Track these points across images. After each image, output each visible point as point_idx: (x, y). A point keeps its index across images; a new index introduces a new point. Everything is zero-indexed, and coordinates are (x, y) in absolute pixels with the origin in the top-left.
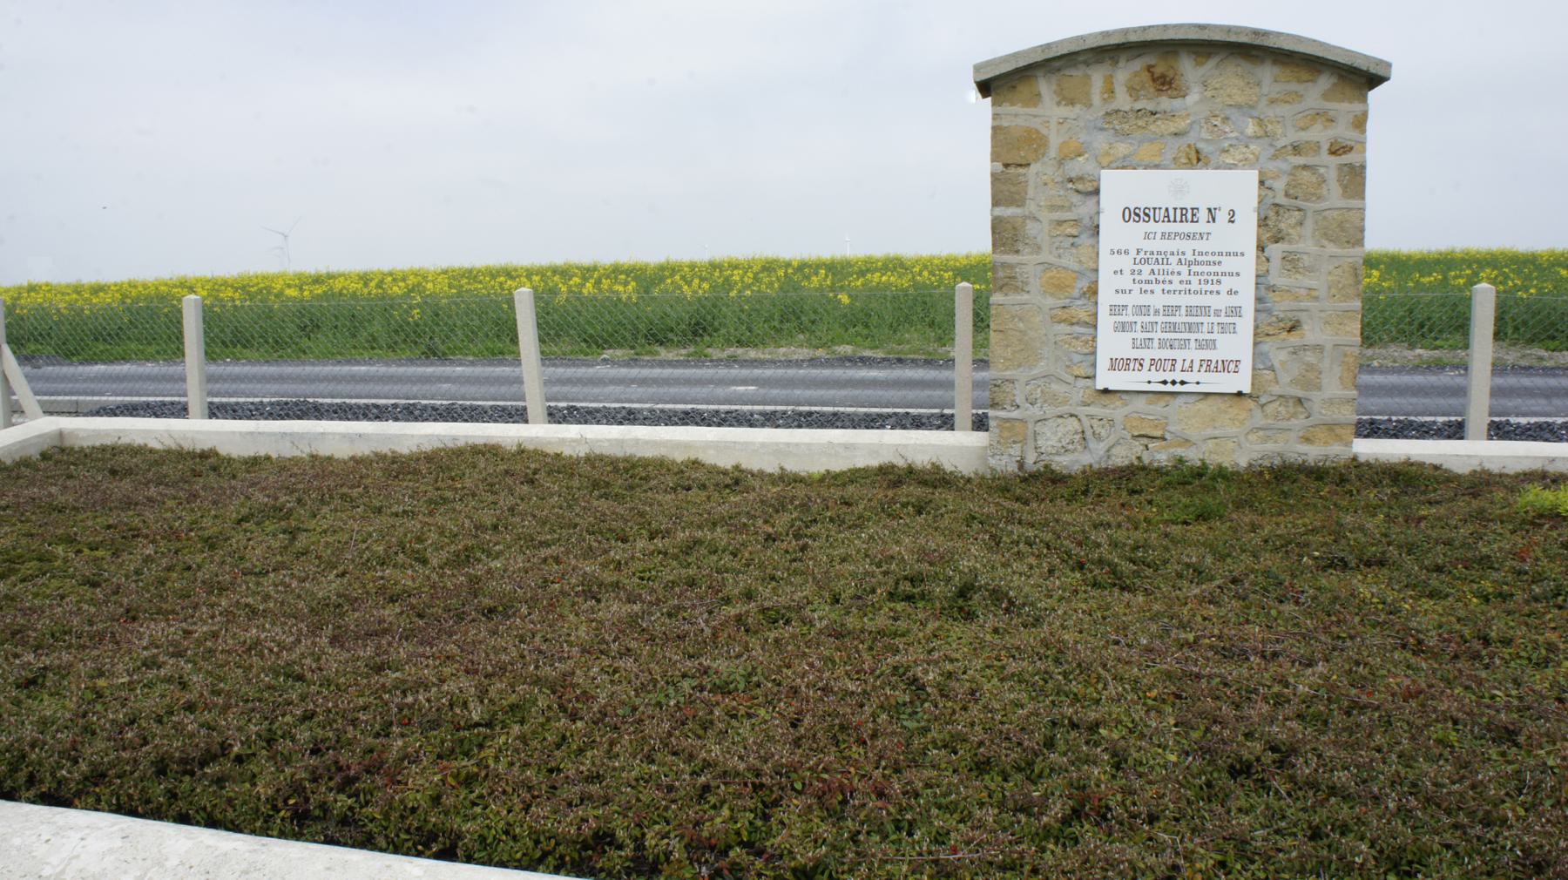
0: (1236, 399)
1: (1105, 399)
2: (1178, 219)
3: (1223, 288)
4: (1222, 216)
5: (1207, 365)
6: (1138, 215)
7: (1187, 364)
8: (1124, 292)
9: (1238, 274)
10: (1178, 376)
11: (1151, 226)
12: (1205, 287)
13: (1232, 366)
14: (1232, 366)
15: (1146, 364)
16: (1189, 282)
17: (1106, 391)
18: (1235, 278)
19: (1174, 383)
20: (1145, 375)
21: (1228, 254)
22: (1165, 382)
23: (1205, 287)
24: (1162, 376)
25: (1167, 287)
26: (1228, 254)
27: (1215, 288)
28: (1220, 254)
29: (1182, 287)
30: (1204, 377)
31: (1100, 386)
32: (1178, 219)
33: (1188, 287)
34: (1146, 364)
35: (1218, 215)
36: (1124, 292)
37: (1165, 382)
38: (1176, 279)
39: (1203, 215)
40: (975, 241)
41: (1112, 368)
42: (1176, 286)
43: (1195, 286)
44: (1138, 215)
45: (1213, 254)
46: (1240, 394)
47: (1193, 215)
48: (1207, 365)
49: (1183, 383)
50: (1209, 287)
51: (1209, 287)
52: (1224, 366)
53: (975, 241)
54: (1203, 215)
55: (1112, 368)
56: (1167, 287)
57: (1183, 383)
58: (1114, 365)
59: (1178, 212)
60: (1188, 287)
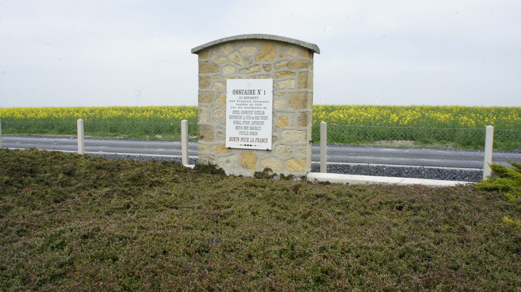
0: (267, 152)
1: (229, 150)
2: (249, 93)
3: (262, 107)
4: (262, 92)
5: (258, 140)
6: (237, 92)
7: (252, 139)
8: (233, 108)
9: (268, 102)
10: (249, 143)
11: (241, 95)
12: (257, 106)
13: (265, 141)
14: (265, 141)
15: (240, 139)
16: (252, 105)
17: (230, 148)
18: (267, 103)
19: (248, 145)
20: (240, 143)
21: (264, 102)
22: (245, 145)
23: (257, 106)
24: (245, 143)
25: (246, 106)
26: (264, 102)
27: (260, 107)
28: (261, 102)
29: (250, 106)
30: (256, 144)
31: (227, 146)
32: (249, 93)
33: (252, 106)
34: (240, 139)
35: (261, 92)
36: (233, 108)
37: (245, 145)
38: (248, 103)
39: (256, 92)
40: (192, 101)
41: (230, 140)
42: (249, 106)
43: (254, 106)
44: (237, 92)
45: (259, 102)
46: (268, 150)
47: (254, 92)
48: (258, 140)
49: (251, 145)
50: (258, 106)
51: (258, 106)
52: (263, 140)
53: (192, 101)
54: (256, 92)
55: (230, 140)
56: (246, 106)
57: (251, 145)
58: (231, 139)
59: (249, 91)
60: (252, 106)
